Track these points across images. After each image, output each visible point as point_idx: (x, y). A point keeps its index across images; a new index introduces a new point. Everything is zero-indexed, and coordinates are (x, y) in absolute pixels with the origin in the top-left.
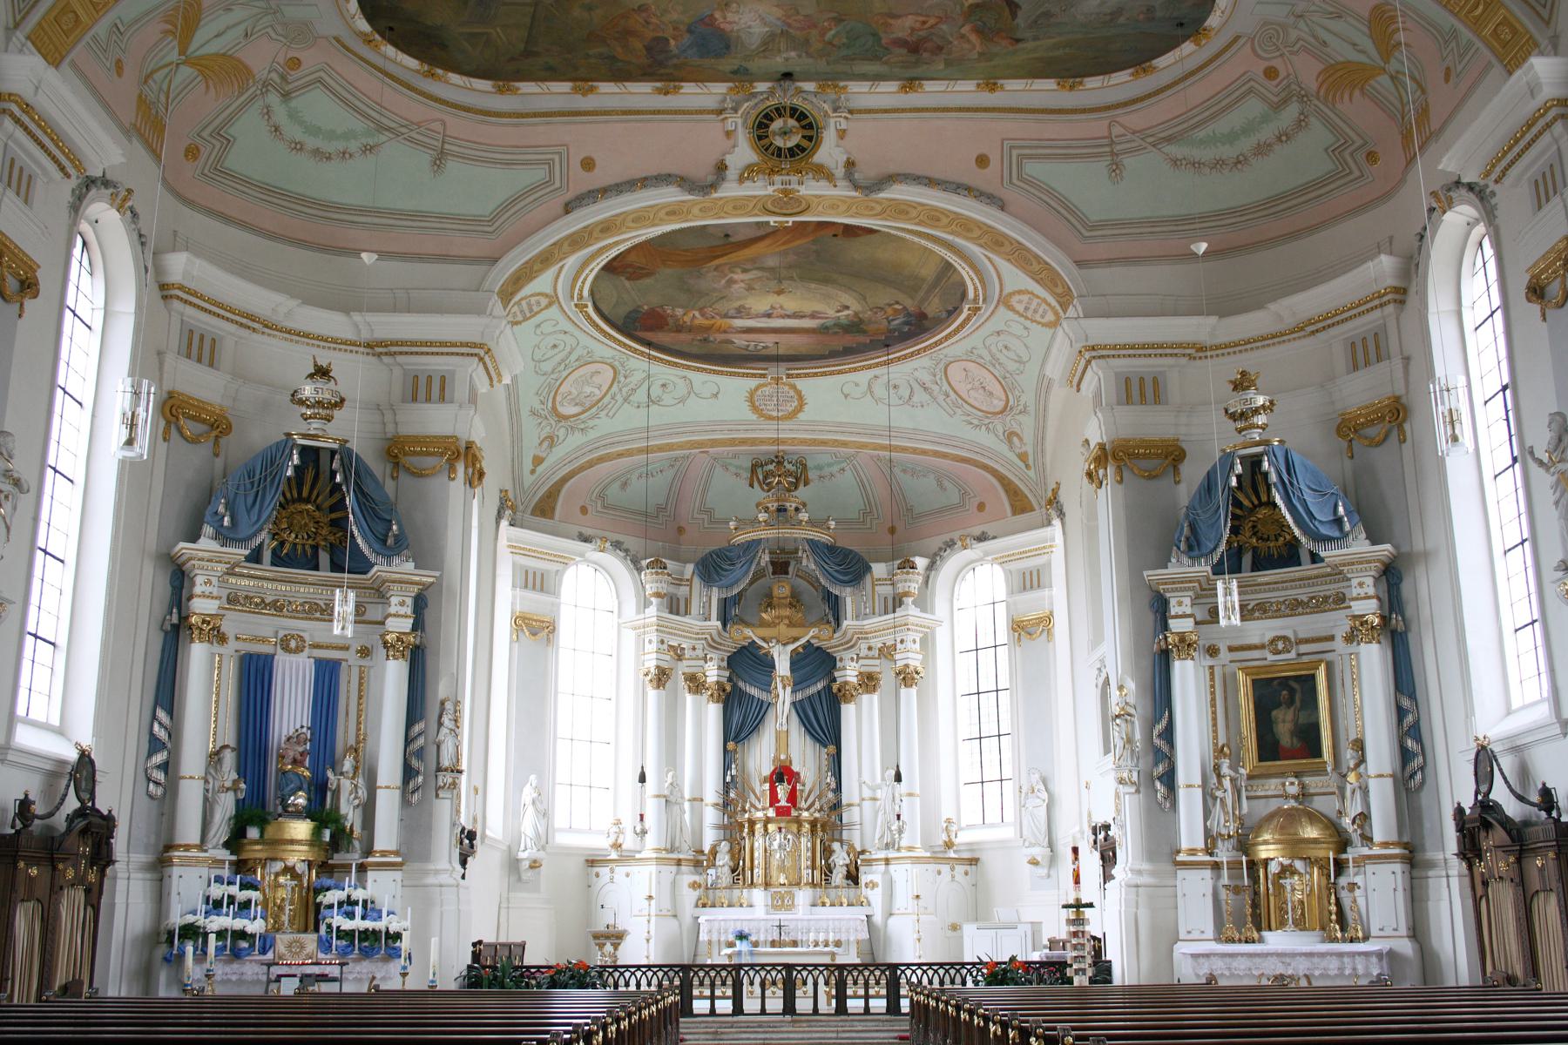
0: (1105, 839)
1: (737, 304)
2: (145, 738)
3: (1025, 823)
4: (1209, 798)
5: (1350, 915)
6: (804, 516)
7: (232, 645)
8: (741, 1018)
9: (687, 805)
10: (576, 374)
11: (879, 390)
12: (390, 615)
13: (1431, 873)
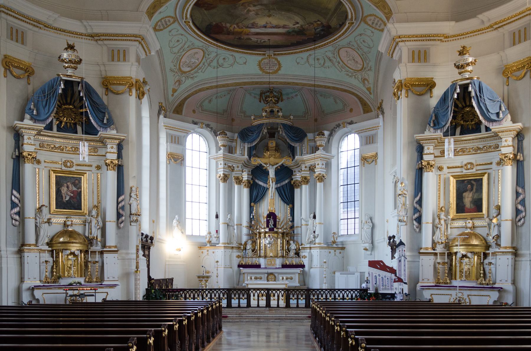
0: (393, 242)
1: (252, 22)
2: (9, 202)
3: (363, 235)
4: (435, 228)
5: (488, 275)
6: (280, 114)
7: (43, 164)
8: (250, 309)
9: (235, 227)
10: (188, 53)
11: (311, 61)
12: (107, 152)
13: (523, 259)
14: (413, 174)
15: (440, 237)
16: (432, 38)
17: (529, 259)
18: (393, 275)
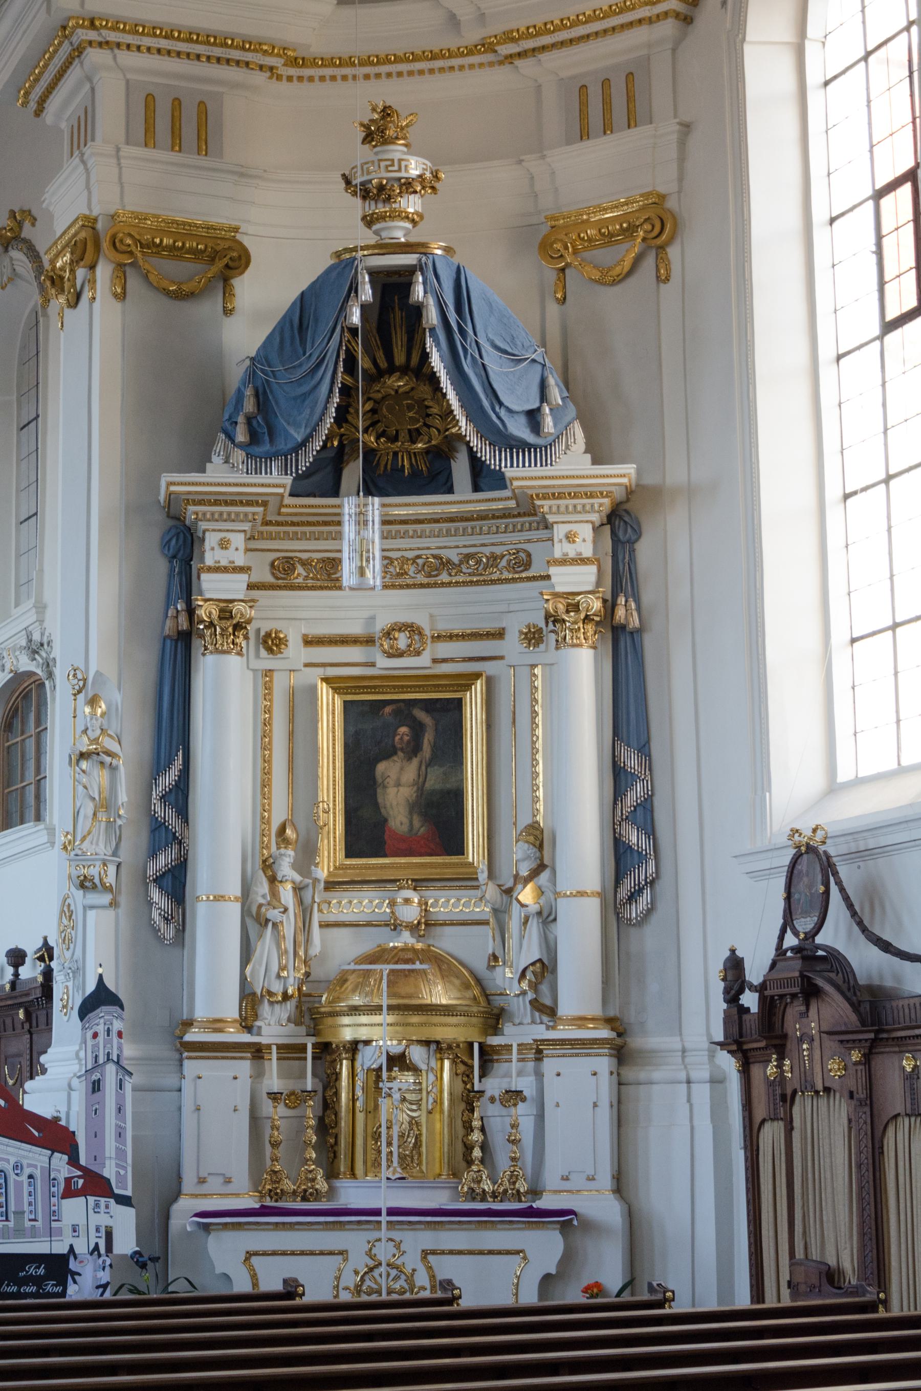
4: (255, 921)
13: (657, 1075)
14: (146, 660)
15: (275, 968)
16: (236, 54)
17: (683, 1076)
18: (60, 1161)
